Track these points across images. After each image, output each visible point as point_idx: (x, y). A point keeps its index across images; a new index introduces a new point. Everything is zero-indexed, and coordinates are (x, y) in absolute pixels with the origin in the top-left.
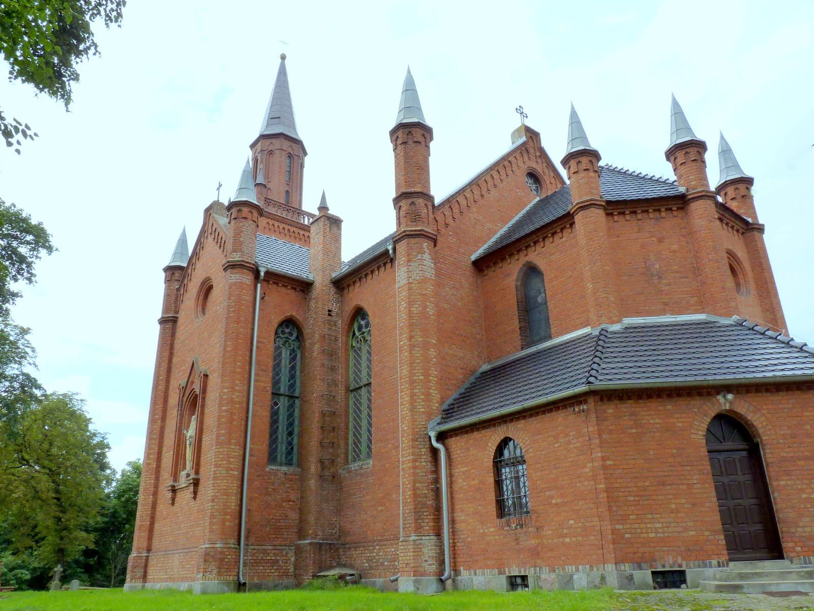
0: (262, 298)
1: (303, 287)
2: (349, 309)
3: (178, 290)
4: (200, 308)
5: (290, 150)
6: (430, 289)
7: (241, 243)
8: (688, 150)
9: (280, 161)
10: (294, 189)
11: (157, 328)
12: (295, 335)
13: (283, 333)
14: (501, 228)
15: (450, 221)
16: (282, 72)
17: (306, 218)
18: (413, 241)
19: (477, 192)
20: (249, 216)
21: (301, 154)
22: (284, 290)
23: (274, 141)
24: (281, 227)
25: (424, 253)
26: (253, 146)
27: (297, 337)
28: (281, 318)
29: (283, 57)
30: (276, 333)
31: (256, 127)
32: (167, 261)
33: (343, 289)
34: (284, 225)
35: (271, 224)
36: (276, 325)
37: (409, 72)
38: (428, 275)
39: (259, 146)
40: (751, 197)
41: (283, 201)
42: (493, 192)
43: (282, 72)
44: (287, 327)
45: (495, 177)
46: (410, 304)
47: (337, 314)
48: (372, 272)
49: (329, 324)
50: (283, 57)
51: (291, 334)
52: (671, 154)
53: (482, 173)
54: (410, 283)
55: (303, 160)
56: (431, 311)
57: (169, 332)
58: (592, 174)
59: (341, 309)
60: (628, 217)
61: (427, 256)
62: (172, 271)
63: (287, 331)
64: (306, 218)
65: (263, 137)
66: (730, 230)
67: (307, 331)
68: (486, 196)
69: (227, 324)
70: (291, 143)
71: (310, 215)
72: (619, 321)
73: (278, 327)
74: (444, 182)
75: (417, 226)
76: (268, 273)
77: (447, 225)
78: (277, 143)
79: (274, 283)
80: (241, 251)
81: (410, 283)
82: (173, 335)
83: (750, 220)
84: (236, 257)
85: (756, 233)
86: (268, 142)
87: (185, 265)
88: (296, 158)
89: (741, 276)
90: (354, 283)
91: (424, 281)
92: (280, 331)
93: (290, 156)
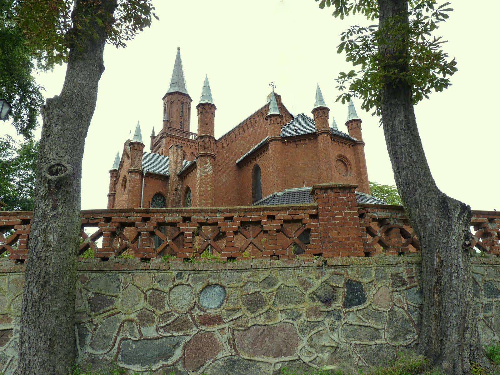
0: (145, 185)
1: (165, 178)
2: (184, 188)
3: (115, 181)
4: (123, 189)
5: (182, 100)
6: (210, 179)
7: (134, 161)
8: (319, 111)
9: (176, 107)
10: (185, 121)
11: (107, 198)
12: (162, 200)
13: (156, 199)
14: (254, 146)
15: (226, 145)
16: (178, 58)
17: (194, 136)
18: (203, 158)
19: (241, 131)
20: (138, 148)
21: (189, 101)
22: (156, 180)
23: (173, 96)
24: (180, 142)
25: (207, 163)
26: (163, 99)
27: (163, 201)
28: (154, 193)
29: (179, 49)
30: (153, 200)
31: (165, 88)
32: (111, 167)
33: (183, 178)
34: (179, 141)
35: (172, 140)
36: (152, 196)
37: (207, 77)
38: (209, 173)
39: (166, 99)
40: (360, 128)
41: (178, 128)
42: (251, 129)
43: (178, 58)
44: (158, 197)
45: (252, 122)
46: (200, 186)
47: (180, 190)
48: (192, 171)
49: (176, 195)
50: (179, 49)
51: (160, 200)
52: (314, 111)
53: (245, 120)
54: (201, 177)
55: (190, 104)
56: (209, 189)
57: (112, 200)
58: (276, 125)
59: (182, 188)
60: (292, 144)
61: (209, 164)
62: (112, 172)
63: (158, 198)
64: (194, 136)
65: (168, 94)
66: (341, 144)
67: (167, 198)
68: (247, 131)
69: (129, 197)
70: (183, 96)
71: (195, 134)
72: (283, 190)
73: (153, 197)
74: (221, 129)
75: (204, 151)
76: (147, 173)
77: (223, 148)
78: (175, 97)
79: (151, 178)
80: (134, 164)
81: (201, 177)
82: (114, 202)
83: (356, 140)
84: (132, 168)
85: (359, 146)
86: (170, 96)
87: (117, 169)
88: (185, 104)
89: (348, 166)
90: (186, 176)
91: (207, 175)
92: (154, 199)
93: (182, 103)
